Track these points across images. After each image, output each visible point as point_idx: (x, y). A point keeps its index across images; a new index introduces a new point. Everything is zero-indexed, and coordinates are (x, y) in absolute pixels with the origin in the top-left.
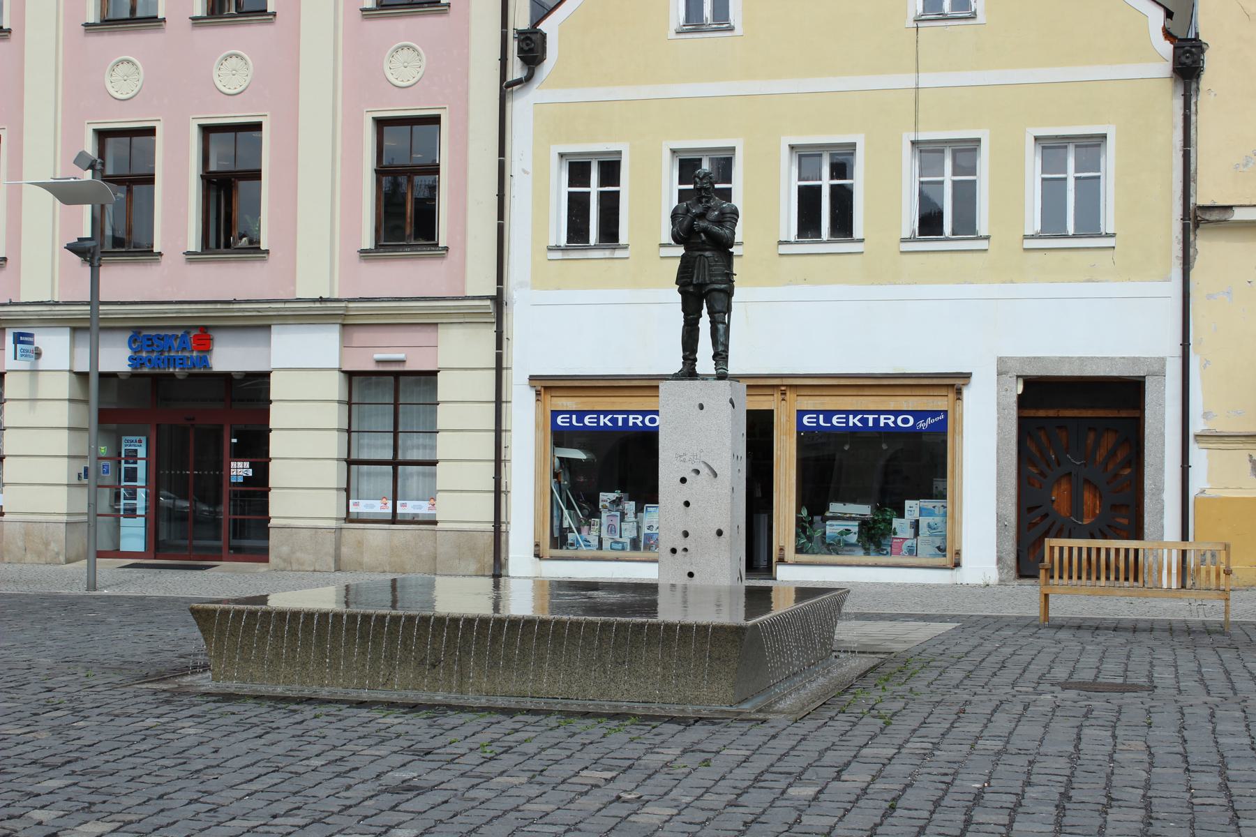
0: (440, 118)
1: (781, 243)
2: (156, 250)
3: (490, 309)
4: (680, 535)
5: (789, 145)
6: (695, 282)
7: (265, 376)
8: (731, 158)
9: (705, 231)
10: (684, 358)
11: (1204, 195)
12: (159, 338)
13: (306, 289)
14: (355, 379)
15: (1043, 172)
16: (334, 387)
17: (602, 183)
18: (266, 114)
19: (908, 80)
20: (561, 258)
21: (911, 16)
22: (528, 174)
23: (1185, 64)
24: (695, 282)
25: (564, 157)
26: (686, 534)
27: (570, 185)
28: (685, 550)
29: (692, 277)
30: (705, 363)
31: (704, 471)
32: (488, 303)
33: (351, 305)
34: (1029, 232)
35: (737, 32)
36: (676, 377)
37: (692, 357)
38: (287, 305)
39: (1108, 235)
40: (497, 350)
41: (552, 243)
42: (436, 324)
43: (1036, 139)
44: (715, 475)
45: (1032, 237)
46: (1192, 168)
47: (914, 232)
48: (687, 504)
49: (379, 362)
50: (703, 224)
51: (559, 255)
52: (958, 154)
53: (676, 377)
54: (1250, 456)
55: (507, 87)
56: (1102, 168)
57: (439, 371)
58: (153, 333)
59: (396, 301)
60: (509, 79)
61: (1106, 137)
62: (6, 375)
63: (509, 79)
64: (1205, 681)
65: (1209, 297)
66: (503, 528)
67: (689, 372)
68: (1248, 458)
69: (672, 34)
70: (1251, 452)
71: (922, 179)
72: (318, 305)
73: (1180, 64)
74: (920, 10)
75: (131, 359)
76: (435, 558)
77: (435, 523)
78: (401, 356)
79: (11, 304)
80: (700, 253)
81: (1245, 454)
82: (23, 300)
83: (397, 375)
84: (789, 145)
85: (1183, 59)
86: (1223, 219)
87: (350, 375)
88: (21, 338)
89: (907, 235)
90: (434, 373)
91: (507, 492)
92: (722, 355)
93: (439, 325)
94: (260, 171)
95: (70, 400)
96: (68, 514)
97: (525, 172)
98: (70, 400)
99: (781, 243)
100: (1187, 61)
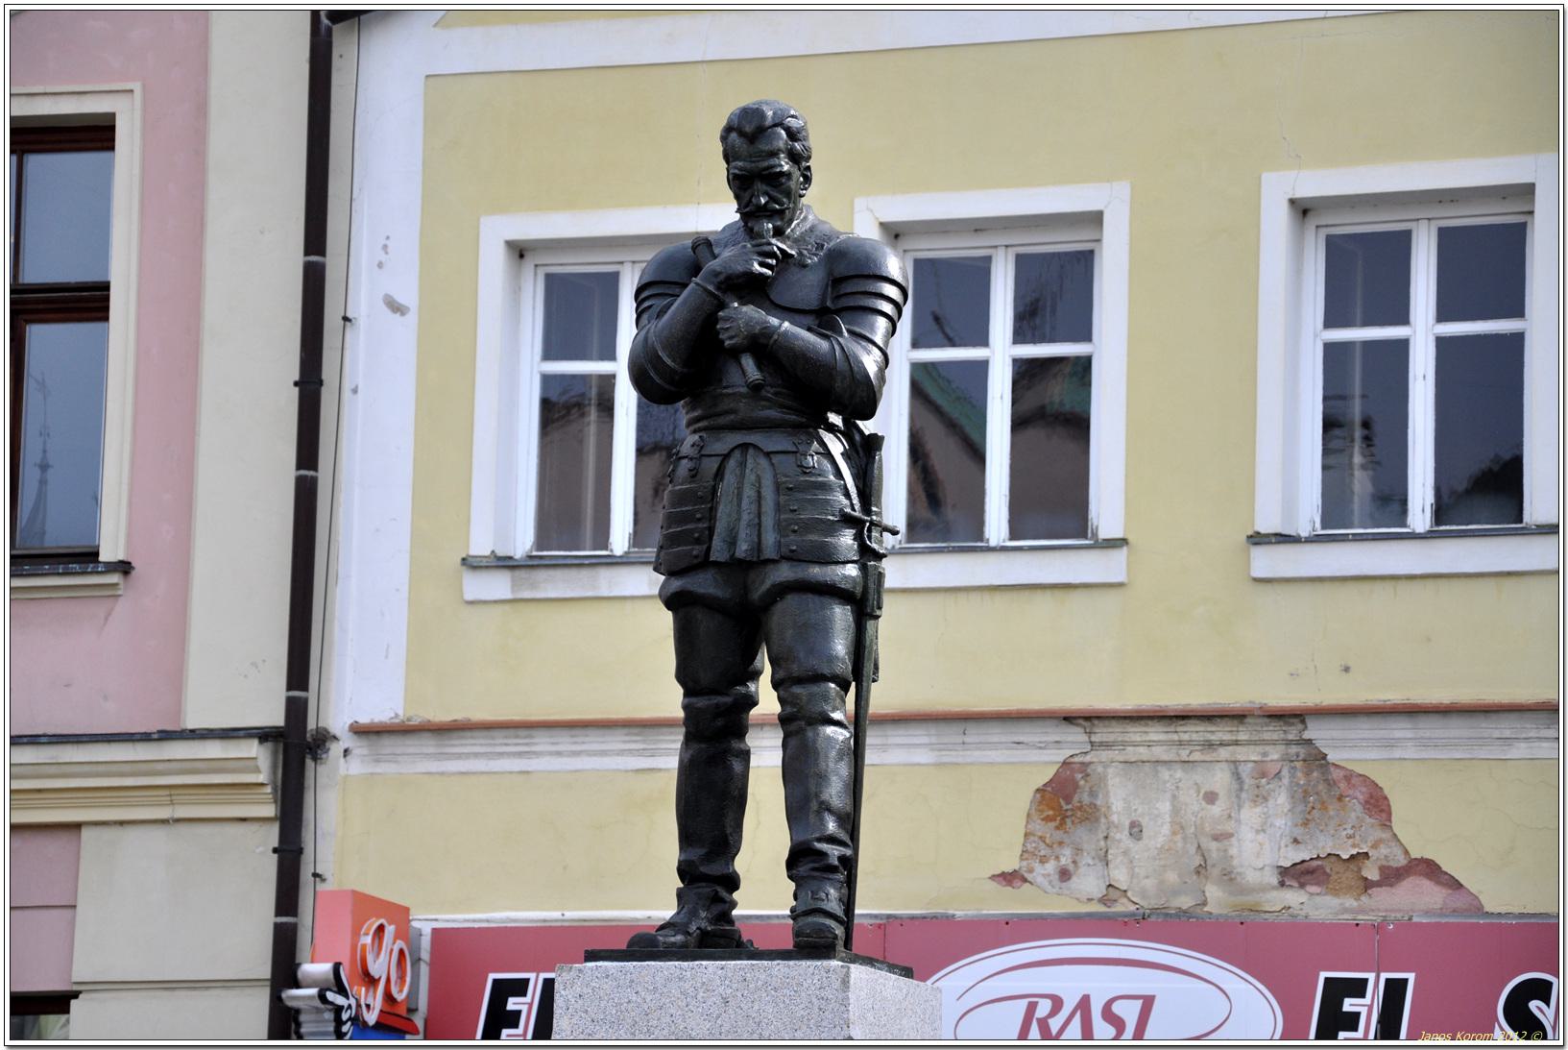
0: (112, 128)
1: (1257, 539)
3: (257, 770)
5: (1292, 202)
6: (718, 552)
8: (1091, 252)
9: (762, 346)
17: (1027, 325)
18: (128, 87)
20: (509, 596)
22: (403, 314)
24: (718, 552)
25: (1310, 215)
27: (548, 355)
32: (252, 749)
36: (643, 946)
37: (714, 869)
40: (278, 914)
41: (481, 546)
42: (77, 827)
50: (747, 314)
51: (498, 586)
53: (643, 946)
57: (75, 995)
59: (57, 743)
62: (73, 1003)
79: (166, 736)
84: (1292, 202)
92: (823, 854)
93: (85, 833)
94: (105, 287)
97: (396, 308)
99: (1257, 539)
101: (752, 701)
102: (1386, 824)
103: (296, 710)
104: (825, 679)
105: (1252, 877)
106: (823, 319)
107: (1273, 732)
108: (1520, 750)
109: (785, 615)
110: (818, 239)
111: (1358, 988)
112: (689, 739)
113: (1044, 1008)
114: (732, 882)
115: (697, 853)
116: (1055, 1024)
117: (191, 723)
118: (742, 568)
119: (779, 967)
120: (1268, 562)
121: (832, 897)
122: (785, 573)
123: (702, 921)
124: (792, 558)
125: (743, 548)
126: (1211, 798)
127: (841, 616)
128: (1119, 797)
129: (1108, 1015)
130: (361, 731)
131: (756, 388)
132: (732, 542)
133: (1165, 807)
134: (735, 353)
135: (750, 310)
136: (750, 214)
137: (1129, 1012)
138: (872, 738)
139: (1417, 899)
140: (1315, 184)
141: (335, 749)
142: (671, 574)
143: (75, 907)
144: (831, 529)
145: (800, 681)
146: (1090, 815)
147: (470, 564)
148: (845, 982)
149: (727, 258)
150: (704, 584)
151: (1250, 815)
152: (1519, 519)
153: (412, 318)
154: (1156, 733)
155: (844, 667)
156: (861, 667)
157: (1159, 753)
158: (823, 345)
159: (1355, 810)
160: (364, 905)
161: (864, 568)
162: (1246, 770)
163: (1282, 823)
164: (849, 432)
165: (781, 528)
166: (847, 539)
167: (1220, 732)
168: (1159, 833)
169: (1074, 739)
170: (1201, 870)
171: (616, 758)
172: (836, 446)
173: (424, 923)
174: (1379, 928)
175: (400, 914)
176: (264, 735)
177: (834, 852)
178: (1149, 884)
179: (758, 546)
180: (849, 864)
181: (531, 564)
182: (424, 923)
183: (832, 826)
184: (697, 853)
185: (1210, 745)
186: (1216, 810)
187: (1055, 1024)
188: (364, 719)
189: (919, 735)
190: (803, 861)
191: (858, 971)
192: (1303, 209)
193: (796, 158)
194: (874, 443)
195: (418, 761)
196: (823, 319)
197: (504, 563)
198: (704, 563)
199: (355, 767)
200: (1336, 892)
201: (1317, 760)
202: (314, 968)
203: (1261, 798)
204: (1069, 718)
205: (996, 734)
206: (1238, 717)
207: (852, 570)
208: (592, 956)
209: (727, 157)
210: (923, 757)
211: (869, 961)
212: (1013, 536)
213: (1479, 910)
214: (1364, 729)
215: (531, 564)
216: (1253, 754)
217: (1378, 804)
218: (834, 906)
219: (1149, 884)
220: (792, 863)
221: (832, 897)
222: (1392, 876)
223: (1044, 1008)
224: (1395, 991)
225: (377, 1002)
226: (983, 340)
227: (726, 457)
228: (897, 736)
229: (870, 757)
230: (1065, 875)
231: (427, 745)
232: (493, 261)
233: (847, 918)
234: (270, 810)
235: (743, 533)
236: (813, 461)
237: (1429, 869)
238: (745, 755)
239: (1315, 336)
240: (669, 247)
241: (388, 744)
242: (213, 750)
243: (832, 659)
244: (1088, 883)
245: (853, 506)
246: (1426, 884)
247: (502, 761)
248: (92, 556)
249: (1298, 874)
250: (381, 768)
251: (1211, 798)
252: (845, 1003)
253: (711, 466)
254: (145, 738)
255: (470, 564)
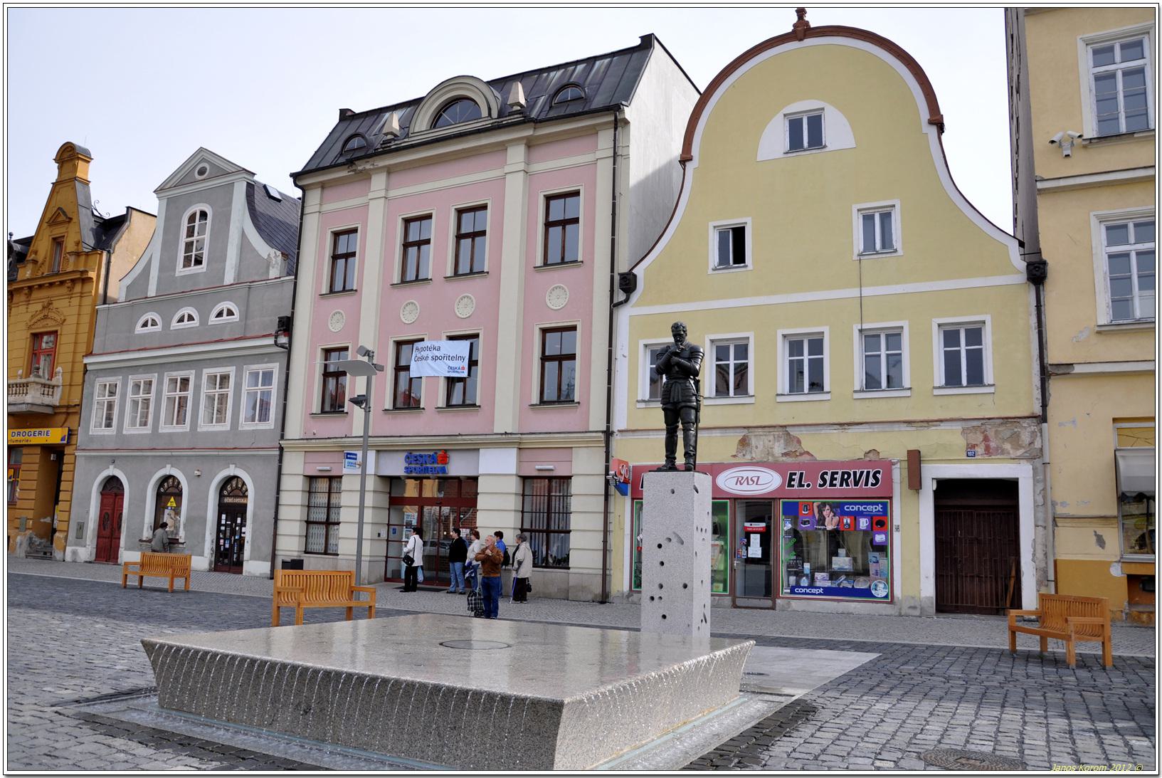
1: (778, 395)
2: (422, 406)
4: (657, 586)
6: (671, 401)
7: (475, 479)
9: (679, 364)
10: (667, 456)
11: (1053, 357)
12: (421, 456)
13: (499, 428)
14: (528, 482)
15: (945, 347)
16: (513, 485)
19: (855, 292)
21: (856, 252)
23: (1035, 275)
24: (671, 401)
26: (661, 586)
28: (661, 598)
29: (669, 398)
30: (680, 460)
31: (674, 540)
32: (601, 434)
33: (524, 436)
34: (937, 385)
35: (749, 268)
37: (672, 456)
38: (488, 437)
39: (989, 385)
41: (640, 399)
42: (572, 448)
43: (939, 325)
44: (682, 543)
45: (940, 388)
46: (1044, 340)
47: (862, 386)
48: (662, 564)
49: (539, 470)
51: (643, 405)
52: (889, 338)
53: (659, 469)
54: (1095, 532)
55: (615, 306)
56: (983, 343)
58: (418, 453)
60: (615, 301)
61: (985, 323)
63: (615, 301)
64: (1079, 754)
65: (1061, 424)
66: (608, 572)
67: (671, 466)
68: (1094, 533)
69: (710, 272)
70: (1096, 529)
71: (867, 354)
72: (504, 436)
73: (1033, 275)
74: (862, 250)
75: (406, 468)
76: (568, 591)
77: (338, 555)
78: (551, 467)
79: (586, 432)
80: (674, 381)
81: (1092, 529)
82: (354, 435)
83: (550, 478)
84: (783, 335)
85: (1034, 272)
86: (1067, 372)
87: (524, 479)
88: (349, 456)
89: (857, 387)
90: (570, 477)
91: (611, 551)
94: (575, 354)
95: (302, 491)
96: (370, 556)
98: (302, 491)
99: (778, 395)
100: (1037, 273)
101: (678, 427)
102: (800, 445)
103: (608, 427)
104: (690, 423)
105: (777, 455)
106: (689, 359)
107: (781, 429)
108: (823, 432)
109: (683, 411)
110: (688, 345)
111: (795, 474)
112: (667, 433)
113: (740, 479)
114: (675, 458)
115: (668, 453)
116: (742, 482)
117: (590, 430)
118: (675, 404)
119: (682, 472)
120: (779, 399)
121: (692, 461)
122: (683, 404)
123: (670, 465)
124: (685, 401)
125: (675, 400)
126: (770, 441)
127: (693, 412)
128: (754, 441)
129: (752, 480)
130: (619, 431)
131: (677, 371)
132: (674, 399)
133: (762, 443)
134: (674, 366)
135: (676, 358)
136: (676, 341)
137: (755, 479)
138: (699, 432)
139: (806, 458)
140: (714, 337)
141: (615, 434)
142: (664, 404)
143: (571, 461)
144: (691, 396)
145: (685, 423)
146: (748, 445)
147: (638, 401)
148: (694, 476)
149: (672, 349)
150: (669, 406)
151: (777, 444)
152: (823, 390)
153: (627, 358)
154: (760, 430)
155: (694, 421)
156: (697, 420)
157: (761, 433)
158: (689, 364)
159: (795, 442)
160: (620, 462)
161: (697, 403)
162: (776, 436)
163: (782, 446)
164: (694, 379)
165: (682, 396)
166: (694, 398)
167: (771, 430)
168: (761, 447)
169: (746, 430)
170: (768, 454)
171: (354, 509)
172: (692, 382)
173: (631, 465)
174: (799, 463)
175: (627, 463)
176: (603, 432)
177: (692, 453)
178: (759, 457)
179: (678, 400)
180: (695, 455)
181: (649, 401)
182: (631, 465)
183: (691, 448)
184: (668, 453)
185: (770, 432)
186: (771, 443)
187: (742, 482)
188: (620, 429)
189: (718, 431)
190: (687, 455)
191: (696, 474)
192: (784, 336)
193: (684, 331)
194: (699, 381)
195: (630, 436)
196: (689, 359)
197: (644, 401)
198: (669, 403)
199: (618, 437)
200: (792, 457)
201: (788, 434)
202: (612, 472)
203: (778, 441)
204: (745, 428)
205: (732, 430)
206: (774, 427)
207: (695, 404)
208: (650, 471)
209: (673, 331)
210: (718, 435)
211: (698, 472)
212: (735, 395)
213: (816, 460)
214: (796, 428)
215: (649, 401)
216: (777, 433)
217: (799, 442)
218: (692, 463)
219: (759, 457)
220: (685, 455)
221: (692, 461)
222: (801, 454)
223: (740, 479)
224: (802, 474)
225: (623, 478)
226: (729, 360)
227: (673, 384)
228: (703, 432)
229: (698, 435)
230: (744, 455)
231: (631, 433)
232: (641, 348)
233: (695, 465)
234: (604, 445)
235: (676, 397)
236: (688, 384)
237: (808, 453)
238: (677, 436)
239: (787, 358)
240: (662, 346)
241: (624, 433)
242: (594, 434)
243: (691, 419)
244: (748, 457)
245: (695, 392)
246: (807, 456)
247: (643, 436)
248: (574, 401)
249: (785, 454)
250: (624, 438)
251: (770, 441)
252: (693, 479)
253: (670, 385)
254: (583, 432)
255: (638, 401)
